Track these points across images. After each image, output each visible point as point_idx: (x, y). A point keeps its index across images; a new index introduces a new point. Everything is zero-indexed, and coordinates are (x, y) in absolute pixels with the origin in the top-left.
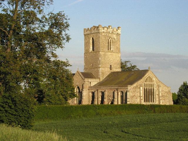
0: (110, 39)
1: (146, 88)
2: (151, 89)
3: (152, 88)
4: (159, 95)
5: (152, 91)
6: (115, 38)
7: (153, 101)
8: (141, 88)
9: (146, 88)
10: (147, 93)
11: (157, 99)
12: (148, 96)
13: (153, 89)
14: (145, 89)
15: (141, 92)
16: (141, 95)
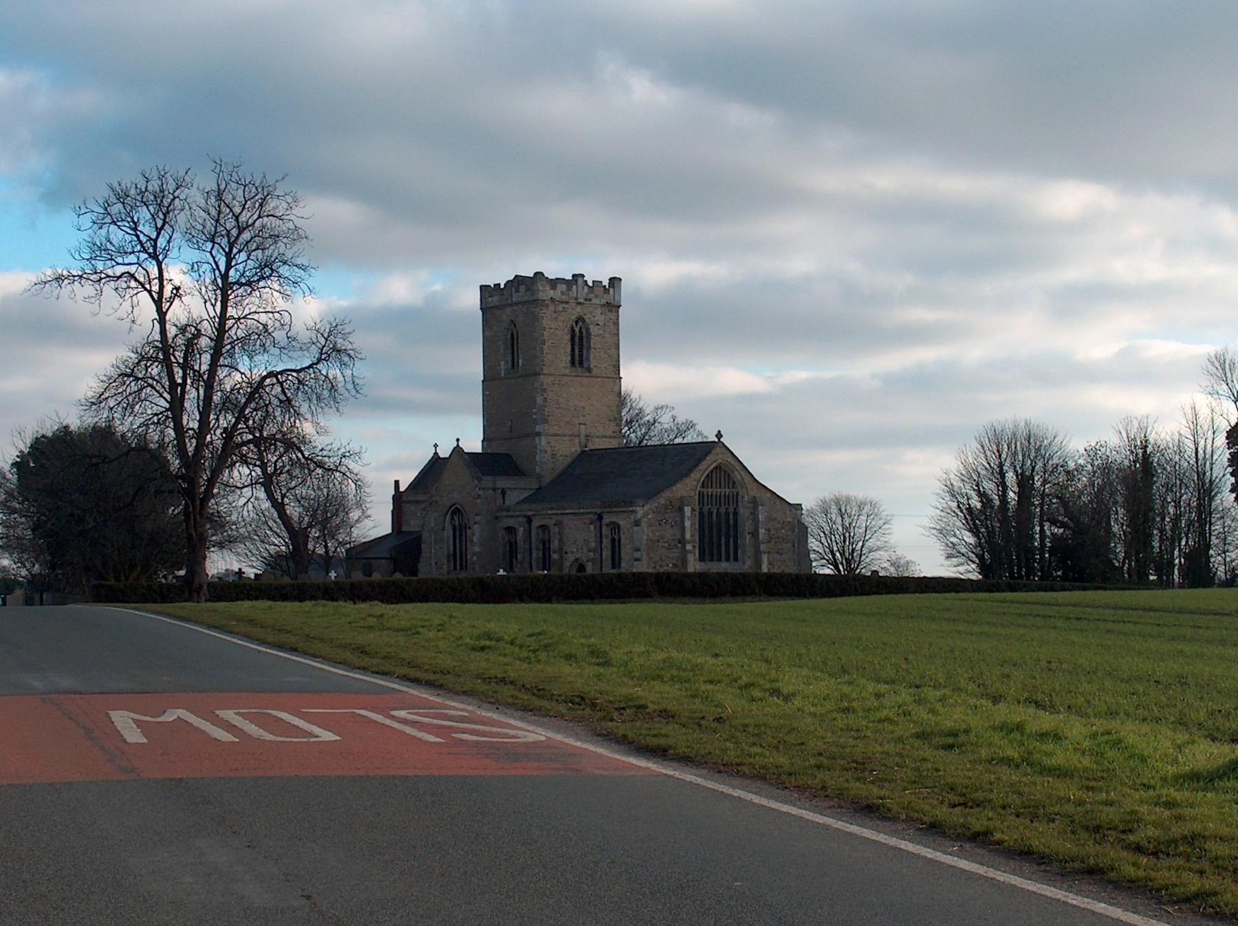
0: (580, 323)
1: (705, 509)
2: (727, 514)
3: (731, 510)
4: (755, 534)
5: (731, 522)
6: (600, 318)
7: (736, 559)
8: (687, 510)
9: (705, 509)
10: (711, 528)
11: (750, 551)
13: (735, 514)
15: (688, 524)
16: (688, 536)
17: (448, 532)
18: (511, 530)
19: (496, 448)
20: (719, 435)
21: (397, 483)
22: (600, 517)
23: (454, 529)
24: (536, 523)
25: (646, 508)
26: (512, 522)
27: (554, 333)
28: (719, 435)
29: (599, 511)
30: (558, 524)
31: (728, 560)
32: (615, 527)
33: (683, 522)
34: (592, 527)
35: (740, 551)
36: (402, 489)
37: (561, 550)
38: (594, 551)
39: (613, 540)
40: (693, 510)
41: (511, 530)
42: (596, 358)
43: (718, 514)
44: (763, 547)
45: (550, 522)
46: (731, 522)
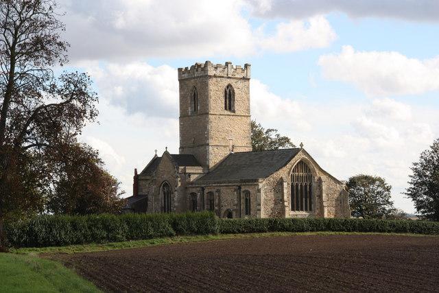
4: (320, 196)
5: (308, 190)
7: (311, 209)
10: (297, 198)
12: (299, 200)
13: (310, 186)
14: (292, 185)
15: (285, 191)
16: (285, 198)
17: (161, 196)
18: (193, 194)
19: (187, 152)
20: (302, 145)
21: (136, 170)
22: (240, 188)
23: (164, 194)
24: (206, 191)
25: (264, 182)
26: (194, 190)
27: (215, 92)
28: (302, 145)
29: (239, 184)
30: (218, 191)
31: (306, 210)
32: (248, 193)
33: (283, 190)
34: (235, 193)
35: (313, 205)
36: (139, 173)
37: (219, 205)
38: (237, 205)
39: (247, 199)
40: (288, 184)
41: (193, 194)
42: (238, 106)
43: (301, 186)
44: (325, 204)
45: (214, 190)
46: (308, 190)
